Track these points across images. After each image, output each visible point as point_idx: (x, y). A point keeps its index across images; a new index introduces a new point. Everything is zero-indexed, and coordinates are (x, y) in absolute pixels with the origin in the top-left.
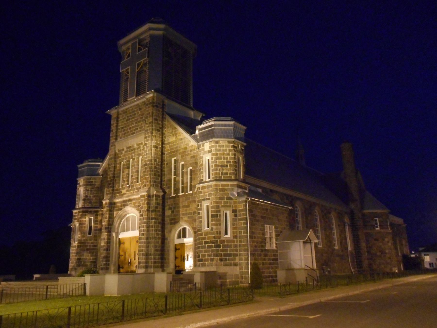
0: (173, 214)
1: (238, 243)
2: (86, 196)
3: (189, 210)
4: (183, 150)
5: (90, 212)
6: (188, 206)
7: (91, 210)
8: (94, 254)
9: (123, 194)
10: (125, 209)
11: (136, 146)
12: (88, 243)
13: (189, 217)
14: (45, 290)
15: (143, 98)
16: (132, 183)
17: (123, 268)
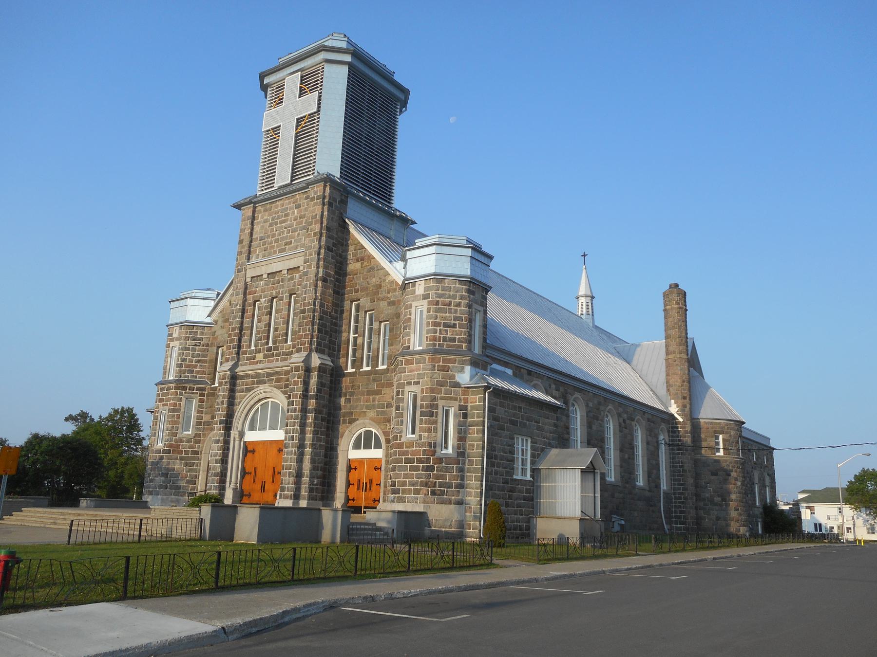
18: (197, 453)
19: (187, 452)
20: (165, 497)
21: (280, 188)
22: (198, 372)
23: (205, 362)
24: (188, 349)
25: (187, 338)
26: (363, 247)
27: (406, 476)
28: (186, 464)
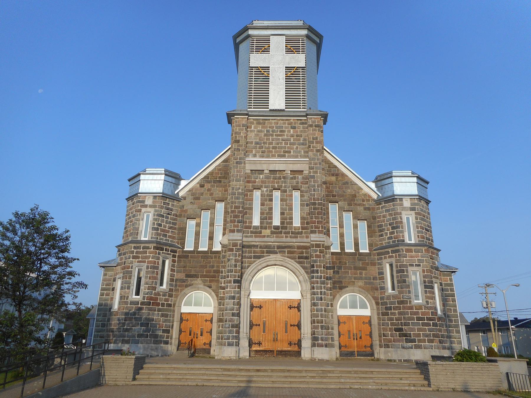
0: (337, 276)
6: (365, 269)
18: (170, 305)
19: (163, 305)
20: (146, 346)
21: (271, 110)
22: (170, 237)
23: (175, 229)
24: (163, 216)
25: (162, 207)
26: (336, 167)
27: (419, 330)
28: (163, 315)
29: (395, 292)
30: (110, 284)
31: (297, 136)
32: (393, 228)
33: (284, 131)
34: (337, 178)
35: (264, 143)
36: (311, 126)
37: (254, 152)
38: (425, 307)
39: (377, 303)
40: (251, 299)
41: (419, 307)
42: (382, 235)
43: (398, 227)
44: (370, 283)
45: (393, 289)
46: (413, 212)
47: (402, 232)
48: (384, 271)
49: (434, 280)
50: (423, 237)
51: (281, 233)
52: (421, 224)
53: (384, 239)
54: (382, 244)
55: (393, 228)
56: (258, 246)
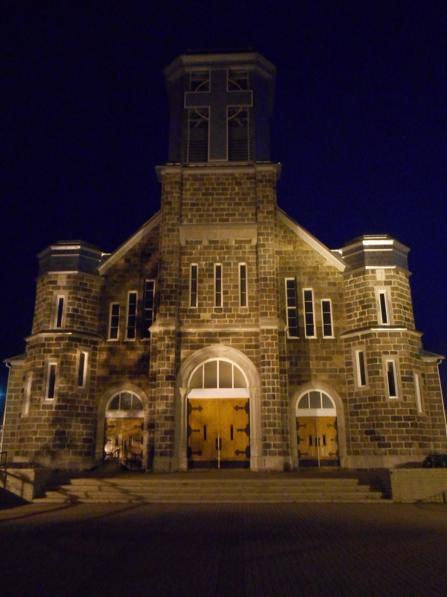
0: (295, 368)
1: (431, 423)
2: (76, 310)
3: (331, 365)
4: (312, 270)
5: (85, 341)
6: (329, 358)
7: (86, 337)
8: (90, 425)
9: (203, 321)
10: (209, 347)
11: (233, 243)
12: (79, 402)
13: (331, 376)
14: (442, 498)
15: (249, 166)
16: (226, 304)
17: (200, 453)
29: (367, 387)
30: (19, 383)
31: (243, 195)
32: (364, 307)
33: (227, 189)
34: (294, 247)
35: (203, 204)
36: (261, 181)
37: (190, 217)
38: (402, 404)
39: (345, 401)
40: (188, 399)
41: (396, 404)
42: (350, 317)
43: (369, 306)
44: (336, 377)
45: (363, 383)
46: (389, 287)
47: (375, 312)
48: (353, 361)
49: (414, 370)
50: (401, 318)
51: (224, 316)
52: (399, 301)
53: (353, 322)
54: (351, 327)
55: (364, 307)
56: (195, 333)
